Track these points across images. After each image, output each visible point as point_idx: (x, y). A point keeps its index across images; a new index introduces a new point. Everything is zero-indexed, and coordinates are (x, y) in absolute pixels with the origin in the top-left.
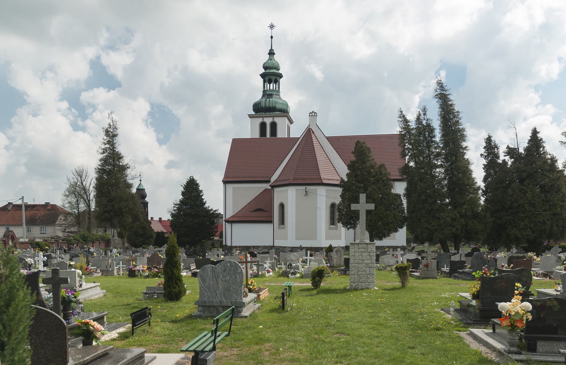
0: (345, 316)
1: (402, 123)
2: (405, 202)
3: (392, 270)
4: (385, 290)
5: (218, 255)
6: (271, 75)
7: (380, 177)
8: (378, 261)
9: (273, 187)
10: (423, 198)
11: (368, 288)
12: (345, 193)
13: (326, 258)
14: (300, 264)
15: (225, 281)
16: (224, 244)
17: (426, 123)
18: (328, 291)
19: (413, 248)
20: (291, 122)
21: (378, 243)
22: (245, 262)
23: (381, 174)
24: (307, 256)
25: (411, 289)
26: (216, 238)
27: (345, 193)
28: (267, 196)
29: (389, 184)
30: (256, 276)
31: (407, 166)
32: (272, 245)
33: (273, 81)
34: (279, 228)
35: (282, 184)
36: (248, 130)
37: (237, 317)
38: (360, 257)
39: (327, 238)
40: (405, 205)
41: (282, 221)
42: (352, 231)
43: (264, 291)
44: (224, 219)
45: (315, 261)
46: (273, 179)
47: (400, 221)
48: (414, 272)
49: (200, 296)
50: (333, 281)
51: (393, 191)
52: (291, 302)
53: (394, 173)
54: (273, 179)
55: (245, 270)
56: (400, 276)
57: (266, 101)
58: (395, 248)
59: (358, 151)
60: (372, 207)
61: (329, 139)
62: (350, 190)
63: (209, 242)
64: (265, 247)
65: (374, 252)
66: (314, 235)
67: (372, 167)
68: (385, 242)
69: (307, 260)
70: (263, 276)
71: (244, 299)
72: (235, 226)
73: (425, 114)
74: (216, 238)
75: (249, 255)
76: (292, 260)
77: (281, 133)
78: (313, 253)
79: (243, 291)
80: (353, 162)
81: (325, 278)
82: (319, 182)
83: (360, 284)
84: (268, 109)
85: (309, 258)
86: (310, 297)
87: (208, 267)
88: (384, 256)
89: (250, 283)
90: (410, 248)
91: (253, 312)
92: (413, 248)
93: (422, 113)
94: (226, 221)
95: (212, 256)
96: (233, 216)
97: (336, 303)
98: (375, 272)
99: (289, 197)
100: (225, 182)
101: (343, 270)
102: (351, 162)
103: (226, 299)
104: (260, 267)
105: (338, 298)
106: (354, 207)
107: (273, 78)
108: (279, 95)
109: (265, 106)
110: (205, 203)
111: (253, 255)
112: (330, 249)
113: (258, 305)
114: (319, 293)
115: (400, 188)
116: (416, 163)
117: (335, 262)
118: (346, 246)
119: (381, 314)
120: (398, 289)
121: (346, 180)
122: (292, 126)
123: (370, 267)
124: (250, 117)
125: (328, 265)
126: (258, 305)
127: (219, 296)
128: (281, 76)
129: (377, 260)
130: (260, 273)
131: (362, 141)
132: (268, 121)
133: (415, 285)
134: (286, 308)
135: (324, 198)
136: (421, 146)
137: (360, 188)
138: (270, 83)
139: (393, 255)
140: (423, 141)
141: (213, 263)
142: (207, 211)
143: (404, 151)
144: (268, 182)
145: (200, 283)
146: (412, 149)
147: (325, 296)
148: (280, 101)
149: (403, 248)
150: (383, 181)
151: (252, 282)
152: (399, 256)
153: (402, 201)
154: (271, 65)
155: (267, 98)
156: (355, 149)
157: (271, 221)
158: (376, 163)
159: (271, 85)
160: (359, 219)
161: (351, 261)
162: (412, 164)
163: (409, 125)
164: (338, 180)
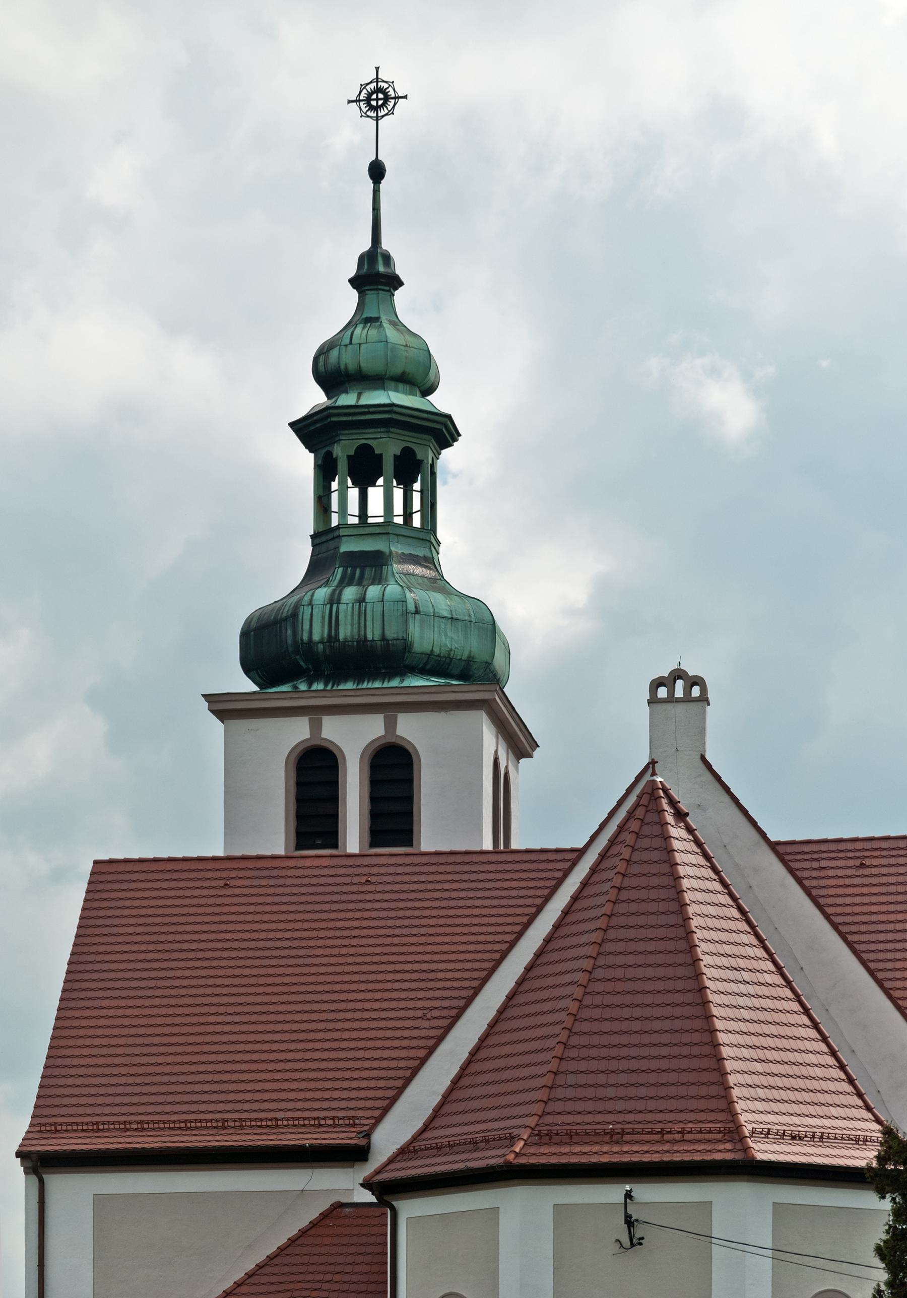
6: (374, 423)
9: (388, 1190)
20: (520, 743)
33: (388, 465)
35: (459, 1167)
36: (201, 799)
46: (389, 1138)
54: (389, 1138)
57: (334, 600)
61: (784, 852)
82: (723, 1153)
84: (353, 660)
100: (39, 1162)
107: (389, 447)
108: (430, 562)
109: (332, 639)
122: (525, 775)
124: (221, 715)
128: (443, 432)
132: (352, 738)
138: (364, 483)
144: (357, 1154)
148: (441, 603)
159: (376, 495)
164: (859, 1141)
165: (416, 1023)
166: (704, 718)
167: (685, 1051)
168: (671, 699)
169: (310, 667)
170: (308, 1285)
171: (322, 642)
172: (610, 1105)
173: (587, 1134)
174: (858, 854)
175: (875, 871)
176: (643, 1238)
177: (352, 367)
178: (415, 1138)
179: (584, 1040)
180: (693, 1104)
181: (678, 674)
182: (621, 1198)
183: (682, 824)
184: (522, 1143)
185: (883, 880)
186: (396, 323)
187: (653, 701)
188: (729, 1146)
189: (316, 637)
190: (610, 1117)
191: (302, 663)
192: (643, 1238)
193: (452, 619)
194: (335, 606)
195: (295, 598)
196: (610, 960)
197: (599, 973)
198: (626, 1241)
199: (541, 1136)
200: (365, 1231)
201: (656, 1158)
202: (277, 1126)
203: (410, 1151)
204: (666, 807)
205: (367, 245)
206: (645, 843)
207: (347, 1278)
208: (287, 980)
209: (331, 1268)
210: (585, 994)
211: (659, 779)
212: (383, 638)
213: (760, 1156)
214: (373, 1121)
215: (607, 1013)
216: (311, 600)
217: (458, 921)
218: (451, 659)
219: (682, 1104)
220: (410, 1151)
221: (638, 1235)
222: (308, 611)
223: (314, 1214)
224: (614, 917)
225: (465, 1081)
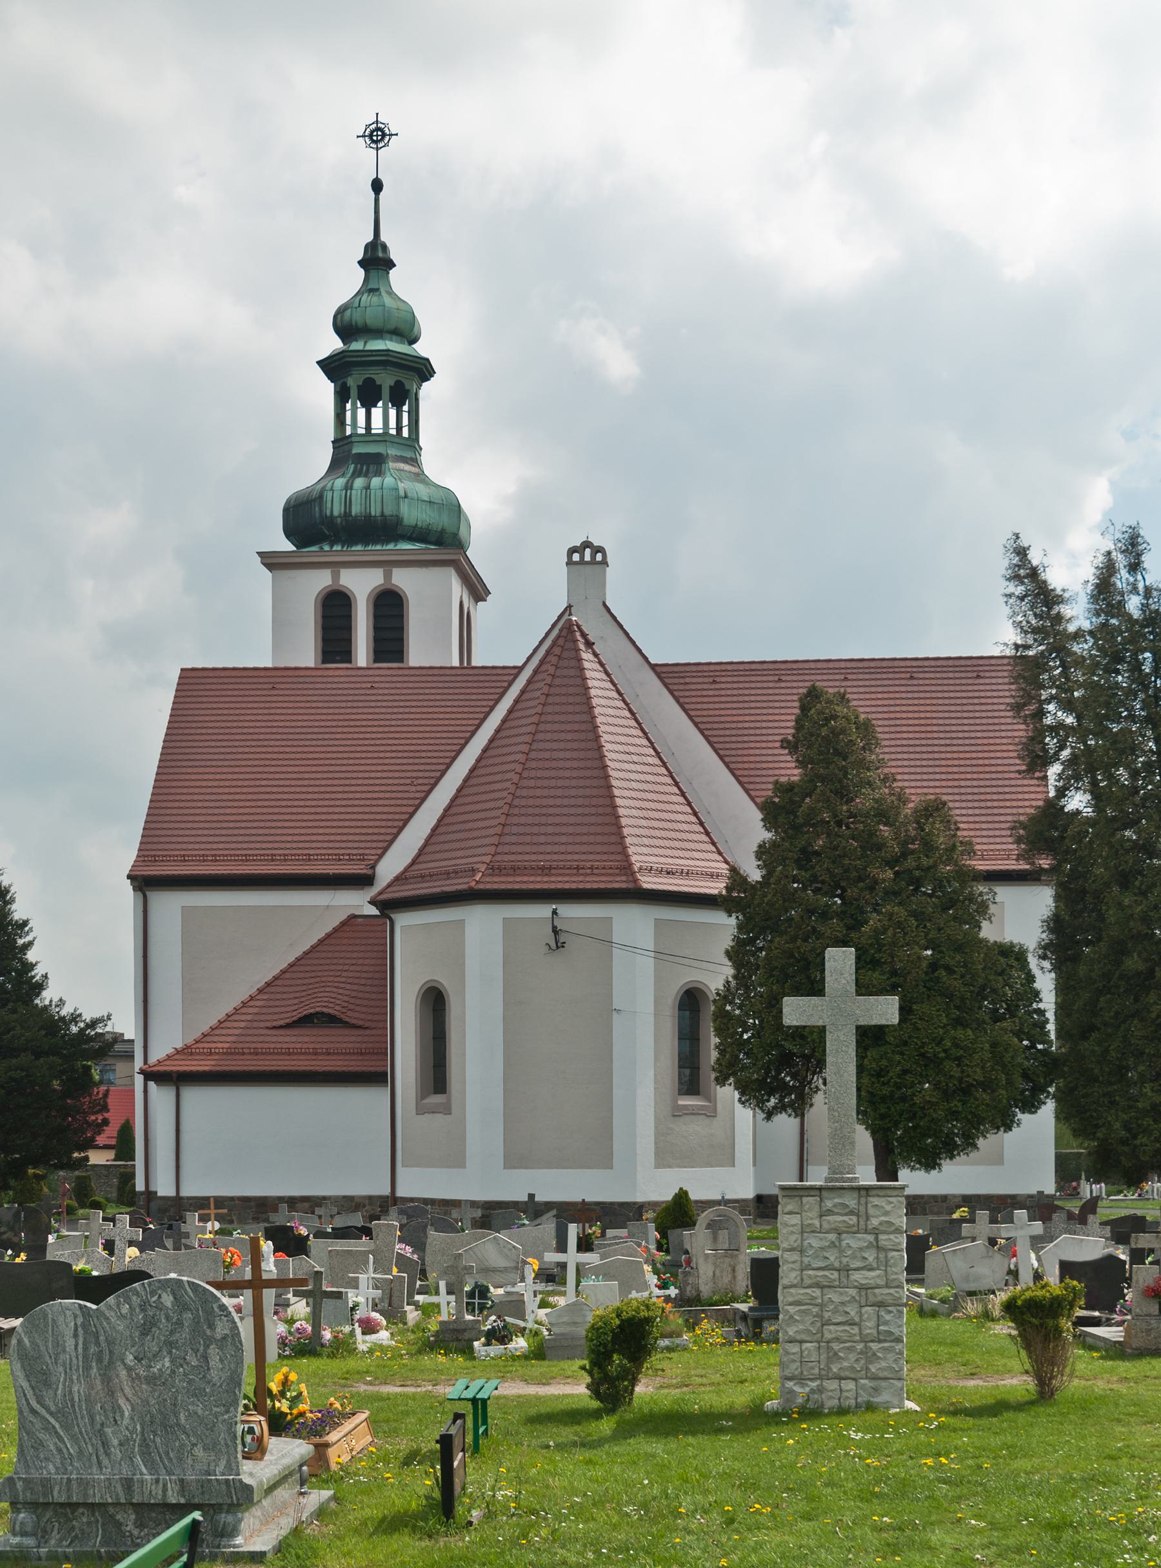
0: (760, 1545)
1: (1025, 606)
2: (1046, 983)
3: (987, 1316)
4: (956, 1412)
5: (109, 1246)
6: (375, 362)
7: (925, 862)
8: (921, 1270)
9: (388, 906)
10: (1133, 963)
11: (870, 1407)
12: (752, 941)
13: (661, 1256)
14: (527, 1288)
15: (151, 1380)
16: (140, 1186)
17: (1144, 607)
18: (671, 1423)
19: (1091, 1206)
20: (477, 590)
21: (915, 1180)
23: (928, 847)
24: (562, 1247)
25: (1086, 1406)
26: (97, 1158)
27: (752, 941)
28: (360, 950)
29: (971, 899)
30: (304, 1347)
31: (1052, 810)
32: (386, 1191)
33: (386, 392)
34: (421, 1110)
36: (257, 626)
37: (213, 1557)
38: (832, 1256)
39: (666, 1156)
40: (1048, 1001)
41: (437, 1075)
42: (786, 1123)
43: (348, 1425)
44: (138, 1063)
45: (604, 1272)
46: (390, 867)
47: (1026, 1076)
48: (1096, 1322)
49: (21, 1452)
50: (683, 1372)
51: (988, 932)
52: (483, 1480)
53: (996, 849)
54: (390, 867)
55: (250, 1321)
56: (1028, 1346)
57: (348, 487)
58: (1000, 1206)
59: (820, 743)
60: (886, 1010)
62: (778, 928)
63: (64, 1180)
64: (350, 1204)
65: (898, 1231)
66: (599, 1152)
67: (884, 814)
68: (954, 1177)
69: (563, 1266)
70: (342, 1347)
71: (247, 1466)
72: (196, 1098)
73: (1135, 567)
74: (97, 1158)
75: (267, 1246)
76: (487, 1270)
77: (426, 648)
78: (596, 1230)
79: (240, 1428)
80: (789, 788)
81: (655, 1360)
83: (832, 1385)
84: (360, 526)
85: (572, 1257)
86: (581, 1455)
87: (64, 1309)
88: (947, 1248)
89: (274, 1387)
90: (1074, 1206)
91: (296, 1532)
92: (1091, 1206)
93: (1121, 561)
94: (150, 1075)
95: (76, 1247)
96: (185, 1052)
97: (711, 1484)
98: (905, 1324)
99: (476, 951)
100: (145, 883)
101: (744, 1317)
102: (779, 788)
103: (152, 1467)
104: (328, 1305)
105: (723, 1454)
106: (796, 1011)
107: (386, 380)
108: (415, 461)
109: (347, 514)
110: (39, 987)
111: (290, 1244)
112: (679, 1213)
113: (318, 1496)
114: (625, 1432)
115: (1021, 917)
116: (1098, 798)
117: (706, 1275)
118: (759, 1198)
119: (936, 1536)
120: (1020, 1407)
121: (755, 874)
122: (481, 613)
123: (881, 1305)
124: (270, 566)
125: (673, 1292)
126: (318, 1496)
127: (117, 1453)
128: (423, 370)
129: (916, 1267)
130: (327, 1335)
131: (831, 689)
132: (362, 584)
133: (1100, 1386)
134: (459, 1510)
135: (649, 969)
136: (1118, 719)
137: (825, 915)
138: (369, 405)
139: (992, 1242)
140: (1131, 693)
141: (94, 1288)
142: (52, 1025)
143: (1037, 737)
144: (364, 881)
145: (21, 1394)
146: (1080, 731)
147: (657, 1447)
149: (1041, 1208)
150: (939, 885)
151: (285, 1383)
152: (1023, 1246)
153: (1031, 978)
154: (371, 317)
155: (356, 474)
156: (799, 726)
157: (379, 1077)
158: (902, 799)
159: (377, 413)
160: (821, 1064)
161: (787, 1275)
162: (1078, 801)
163: (1059, 618)
164: (713, 876)
168: (582, 562)
171: (340, 516)
172: (542, 848)
175: (723, 686)
177: (360, 323)
178: (406, 870)
186: (391, 293)
187: (570, 563)
189: (336, 513)
190: (541, 857)
197: (533, 755)
204: (579, 638)
205: (370, 238)
209: (347, 961)
212: (382, 515)
213: (645, 886)
223: (336, 923)
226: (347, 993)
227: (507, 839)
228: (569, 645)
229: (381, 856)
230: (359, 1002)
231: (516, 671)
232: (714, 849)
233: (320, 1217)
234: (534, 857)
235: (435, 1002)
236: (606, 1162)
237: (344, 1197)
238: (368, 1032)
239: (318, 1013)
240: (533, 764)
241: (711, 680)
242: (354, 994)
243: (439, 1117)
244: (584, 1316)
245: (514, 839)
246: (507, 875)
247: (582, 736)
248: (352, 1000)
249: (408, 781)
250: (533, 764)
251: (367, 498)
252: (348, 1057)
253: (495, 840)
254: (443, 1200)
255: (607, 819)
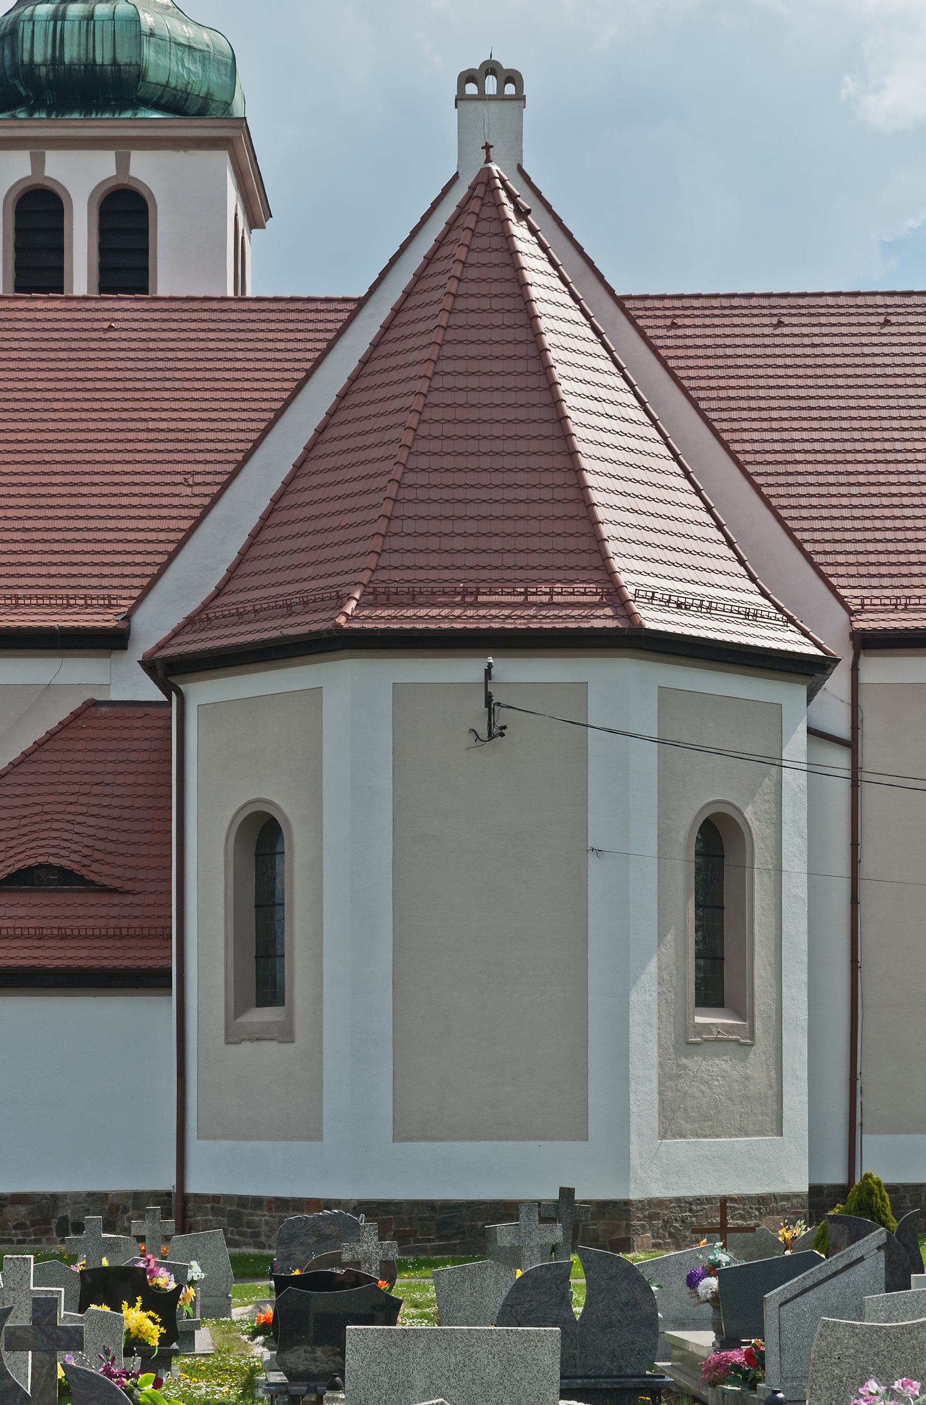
9: (169, 669)
20: (257, 212)
22: (724, 1222)
32: (168, 1183)
34: (233, 1037)
41: (264, 974)
109: (56, 61)
132: (79, 176)
144: (113, 641)
157: (153, 979)
165: (175, 489)
166: (521, 121)
167: (546, 494)
168: (482, 97)
169: (31, 94)
170: (62, 798)
171: (44, 64)
172: (459, 560)
173: (433, 593)
174: (668, 313)
175: (688, 332)
176: (505, 728)
178: (205, 606)
179: (422, 479)
180: (559, 560)
181: (491, 68)
182: (481, 677)
183: (524, 223)
184: (353, 604)
185: (699, 342)
187: (461, 98)
188: (608, 611)
189: (38, 58)
190: (459, 574)
191: (21, 90)
192: (505, 728)
193: (189, 47)
194: (59, 24)
195: (13, 14)
196: (449, 382)
197: (435, 398)
198: (483, 732)
199: (375, 597)
200: (126, 734)
201: (521, 624)
202: (17, 605)
203: (202, 621)
204: (505, 200)
206: (483, 242)
207: (108, 790)
208: (20, 436)
209: (87, 779)
210: (421, 421)
211: (495, 167)
212: (114, 63)
213: (649, 625)
214: (133, 602)
215: (448, 446)
216: (32, 15)
217: (217, 375)
218: (189, 94)
219: (546, 560)
220: (202, 621)
221: (499, 724)
222: (28, 27)
223: (64, 714)
224: (449, 330)
225: (267, 534)
226: (91, 831)
227: (396, 543)
228: (487, 212)
229: (140, 600)
230: (110, 847)
231: (351, 306)
232: (742, 571)
233: (141, 1239)
234: (446, 574)
235: (262, 839)
236: (669, 1128)
237: (90, 1195)
238: (129, 899)
239: (40, 866)
240: (437, 414)
241: (668, 322)
242: (102, 834)
243: (270, 1048)
244: (323, 1352)
245: (408, 543)
246: (401, 605)
247: (521, 366)
248: (99, 845)
249: (179, 479)
250: (437, 414)
251: (90, 33)
252: (97, 943)
253: (376, 544)
254: (277, 1199)
255: (572, 509)
